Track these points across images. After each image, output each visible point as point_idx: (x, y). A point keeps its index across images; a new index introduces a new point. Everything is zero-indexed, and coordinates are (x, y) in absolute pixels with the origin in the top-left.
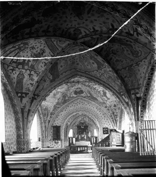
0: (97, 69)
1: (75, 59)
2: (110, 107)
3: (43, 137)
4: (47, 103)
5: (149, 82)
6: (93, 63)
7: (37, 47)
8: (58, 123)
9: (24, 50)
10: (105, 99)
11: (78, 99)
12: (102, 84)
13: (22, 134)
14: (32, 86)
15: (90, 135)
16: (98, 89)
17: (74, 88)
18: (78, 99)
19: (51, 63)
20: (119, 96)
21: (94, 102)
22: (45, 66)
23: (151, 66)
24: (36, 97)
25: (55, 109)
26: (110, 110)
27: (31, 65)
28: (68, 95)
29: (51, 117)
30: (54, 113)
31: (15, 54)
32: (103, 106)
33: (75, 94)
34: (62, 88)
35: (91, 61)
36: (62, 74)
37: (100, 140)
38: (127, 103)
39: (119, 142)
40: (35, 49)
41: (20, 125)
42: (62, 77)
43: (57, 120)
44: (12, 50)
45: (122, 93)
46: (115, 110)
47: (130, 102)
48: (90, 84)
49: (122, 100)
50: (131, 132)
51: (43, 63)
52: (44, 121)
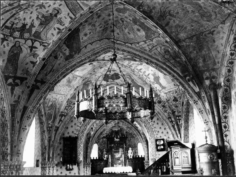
0: (145, 39)
1: (108, 24)
2: (168, 101)
3: (45, 159)
5: (231, 59)
6: (139, 30)
7: (48, 5)
8: (73, 132)
9: (26, 9)
12: (153, 63)
13: (9, 153)
14: (33, 67)
15: (130, 154)
16: (145, 72)
17: (103, 69)
19: (70, 30)
20: (184, 83)
22: (58, 33)
23: (233, 35)
24: (39, 84)
26: (167, 106)
27: (36, 32)
28: (93, 82)
29: (60, 120)
30: (67, 114)
31: (11, 15)
34: (83, 70)
35: (136, 27)
36: (86, 47)
37: (151, 163)
38: (199, 95)
39: (188, 165)
40: (45, 8)
41: (7, 135)
42: (85, 51)
43: (72, 126)
44: (7, 10)
45: (188, 78)
47: (202, 93)
48: (131, 64)
49: (189, 89)
50: (209, 145)
51: (55, 29)
52: (47, 128)
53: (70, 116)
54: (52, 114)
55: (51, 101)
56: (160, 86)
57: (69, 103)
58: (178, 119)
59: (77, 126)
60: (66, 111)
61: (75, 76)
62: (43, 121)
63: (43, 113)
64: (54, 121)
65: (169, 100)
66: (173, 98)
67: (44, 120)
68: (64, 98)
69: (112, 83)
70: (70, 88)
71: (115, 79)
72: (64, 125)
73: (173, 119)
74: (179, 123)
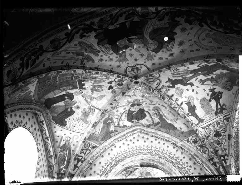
4: (68, 133)
10: (194, 122)
11: (136, 130)
16: (177, 99)
18: (136, 130)
21: (168, 133)
25: (87, 150)
29: (76, 166)
30: (85, 159)
32: (188, 141)
33: (128, 120)
46: (220, 143)
53: (89, 161)
54: (65, 158)
55: (64, 140)
56: (197, 119)
57: (87, 146)
58: (223, 160)
59: (97, 174)
60: (83, 155)
61: (92, 107)
62: (51, 164)
63: (52, 154)
64: (67, 167)
65: (208, 136)
66: (213, 133)
67: (54, 163)
68: (80, 137)
69: (138, 124)
70: (87, 125)
71: (140, 120)
72: (81, 172)
73: (216, 160)
74: (225, 165)
